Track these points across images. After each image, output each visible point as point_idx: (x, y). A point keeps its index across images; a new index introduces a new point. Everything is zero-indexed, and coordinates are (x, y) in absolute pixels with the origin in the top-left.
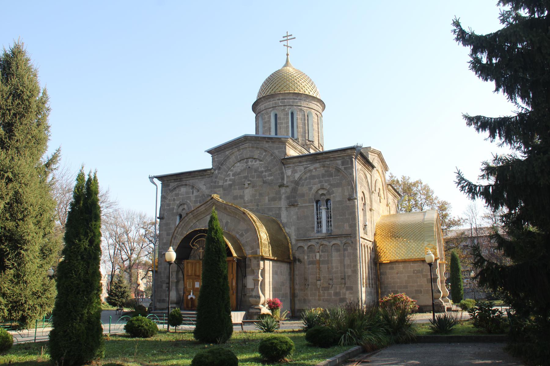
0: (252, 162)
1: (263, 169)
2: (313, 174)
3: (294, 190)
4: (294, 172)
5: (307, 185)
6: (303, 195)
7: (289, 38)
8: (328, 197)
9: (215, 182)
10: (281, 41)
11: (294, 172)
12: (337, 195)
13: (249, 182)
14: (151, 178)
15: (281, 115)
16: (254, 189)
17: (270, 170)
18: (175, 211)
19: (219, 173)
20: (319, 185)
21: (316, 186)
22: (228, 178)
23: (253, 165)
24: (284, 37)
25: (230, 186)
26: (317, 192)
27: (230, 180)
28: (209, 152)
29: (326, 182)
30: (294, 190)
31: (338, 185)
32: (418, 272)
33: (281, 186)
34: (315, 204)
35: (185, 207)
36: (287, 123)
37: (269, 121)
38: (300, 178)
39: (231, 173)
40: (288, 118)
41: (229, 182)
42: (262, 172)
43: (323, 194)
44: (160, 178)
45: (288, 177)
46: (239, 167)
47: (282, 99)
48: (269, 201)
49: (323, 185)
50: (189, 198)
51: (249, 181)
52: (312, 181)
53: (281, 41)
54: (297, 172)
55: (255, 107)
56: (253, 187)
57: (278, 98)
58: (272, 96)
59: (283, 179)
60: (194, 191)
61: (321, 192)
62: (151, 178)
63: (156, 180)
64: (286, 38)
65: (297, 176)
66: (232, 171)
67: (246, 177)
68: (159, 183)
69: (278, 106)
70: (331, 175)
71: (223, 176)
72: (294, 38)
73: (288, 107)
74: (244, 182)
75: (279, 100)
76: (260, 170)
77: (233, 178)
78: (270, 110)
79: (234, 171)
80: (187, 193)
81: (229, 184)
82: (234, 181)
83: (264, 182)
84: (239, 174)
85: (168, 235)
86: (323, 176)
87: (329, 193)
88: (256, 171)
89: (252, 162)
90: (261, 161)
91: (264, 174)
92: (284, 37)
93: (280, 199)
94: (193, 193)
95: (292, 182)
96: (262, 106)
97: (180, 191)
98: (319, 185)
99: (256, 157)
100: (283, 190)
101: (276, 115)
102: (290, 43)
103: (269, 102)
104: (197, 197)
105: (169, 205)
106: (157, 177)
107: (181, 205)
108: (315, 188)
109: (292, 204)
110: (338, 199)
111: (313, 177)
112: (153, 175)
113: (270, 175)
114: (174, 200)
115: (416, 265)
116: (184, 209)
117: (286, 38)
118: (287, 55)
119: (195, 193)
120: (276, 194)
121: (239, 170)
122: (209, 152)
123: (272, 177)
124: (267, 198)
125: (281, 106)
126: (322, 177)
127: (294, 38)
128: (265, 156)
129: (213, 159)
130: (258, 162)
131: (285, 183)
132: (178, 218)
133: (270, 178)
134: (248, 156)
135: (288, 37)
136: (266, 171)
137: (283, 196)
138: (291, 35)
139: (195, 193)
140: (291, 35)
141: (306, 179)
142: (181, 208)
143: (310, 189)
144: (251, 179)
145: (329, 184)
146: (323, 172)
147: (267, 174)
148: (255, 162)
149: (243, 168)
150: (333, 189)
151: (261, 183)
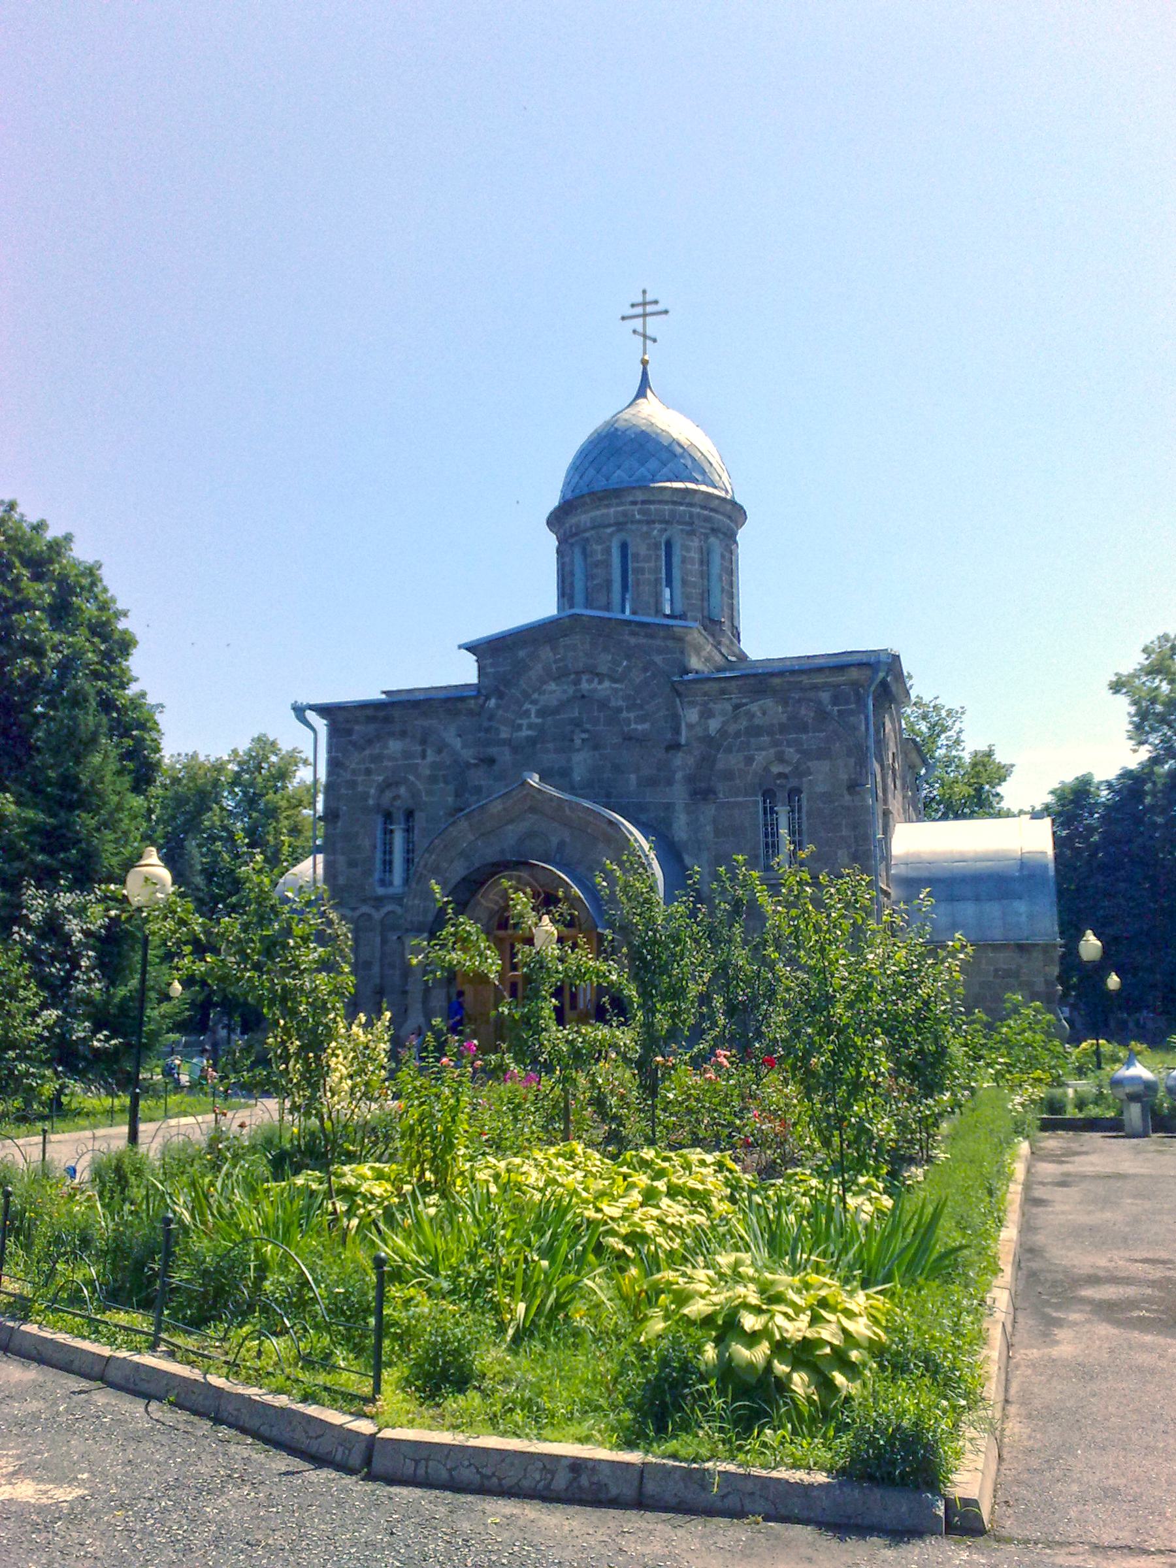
0: (590, 681)
1: (621, 703)
2: (757, 721)
3: (707, 761)
4: (706, 714)
5: (739, 751)
6: (728, 775)
7: (649, 309)
8: (794, 782)
9: (488, 730)
10: (623, 318)
11: (706, 714)
12: (821, 777)
13: (585, 736)
14: (299, 711)
15: (639, 547)
16: (596, 753)
17: (641, 707)
18: (371, 802)
19: (498, 706)
20: (772, 751)
21: (764, 753)
22: (524, 722)
23: (595, 690)
24: (633, 306)
25: (532, 741)
26: (766, 769)
27: (530, 727)
28: (471, 648)
29: (789, 746)
30: (707, 761)
31: (824, 753)
32: (1008, 974)
33: (674, 746)
34: (760, 799)
35: (402, 790)
36: (657, 570)
37: (607, 564)
38: (722, 732)
39: (533, 709)
40: (658, 557)
41: (525, 733)
42: (619, 710)
43: (781, 775)
44: (324, 710)
45: (690, 726)
46: (554, 692)
47: (643, 502)
48: (639, 785)
49: (783, 752)
50: (414, 769)
51: (584, 731)
52: (752, 740)
53: (623, 318)
54: (714, 716)
55: (556, 520)
56: (596, 747)
57: (631, 499)
58: (614, 494)
59: (677, 731)
60: (429, 752)
61: (775, 769)
62: (299, 711)
63: (311, 716)
64: (639, 310)
65: (714, 725)
66: (534, 702)
67: (577, 723)
68: (320, 724)
69: (632, 522)
70: (804, 728)
71: (509, 715)
72: (666, 312)
73: (657, 526)
74: (573, 732)
75: (634, 503)
76: (613, 704)
77: (540, 720)
78: (609, 530)
79: (542, 703)
80: (407, 755)
81: (528, 738)
82: (541, 729)
83: (628, 738)
84: (556, 711)
85: (352, 864)
86: (783, 729)
87: (799, 773)
88: (603, 705)
89: (590, 681)
90: (615, 681)
91: (625, 714)
92: (633, 306)
93: (670, 782)
94: (424, 757)
95: (698, 739)
96: (583, 518)
97: (386, 747)
98: (772, 751)
99: (603, 669)
100: (679, 759)
101: (624, 547)
102: (654, 325)
103: (608, 506)
104: (434, 766)
105: (352, 784)
106: (312, 708)
107: (389, 786)
108: (760, 758)
109: (701, 793)
110: (820, 788)
111: (755, 731)
112: (305, 699)
113: (641, 719)
114: (368, 772)
115: (1001, 956)
116: (396, 797)
117: (639, 310)
118: (645, 363)
119: (431, 756)
120: (659, 770)
121: (555, 703)
122: (471, 648)
123: (647, 726)
124: (633, 777)
125: (639, 522)
126: (781, 733)
127: (666, 312)
128: (628, 669)
129: (480, 669)
130: (607, 684)
131: (683, 741)
132: (379, 819)
133: (639, 727)
134: (580, 665)
135: (645, 308)
136: (629, 709)
137: (679, 776)
138: (656, 302)
139: (431, 756)
140: (656, 302)
141: (738, 734)
142: (388, 795)
143: (749, 760)
144: (588, 726)
145: (798, 751)
146: (784, 718)
147: (632, 715)
148: (600, 683)
149: (564, 697)
150: (809, 764)
151: (616, 740)
